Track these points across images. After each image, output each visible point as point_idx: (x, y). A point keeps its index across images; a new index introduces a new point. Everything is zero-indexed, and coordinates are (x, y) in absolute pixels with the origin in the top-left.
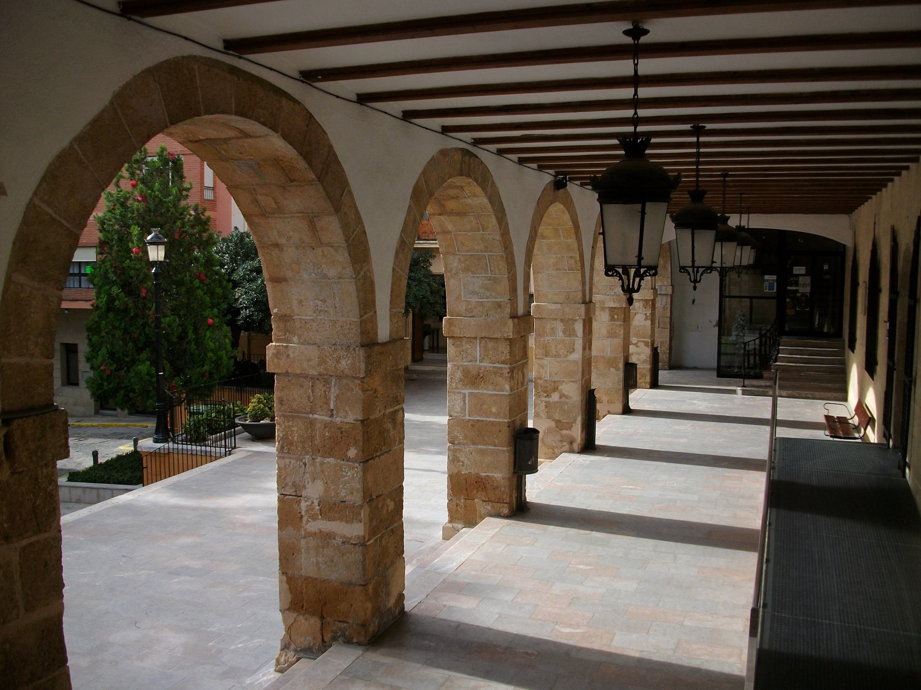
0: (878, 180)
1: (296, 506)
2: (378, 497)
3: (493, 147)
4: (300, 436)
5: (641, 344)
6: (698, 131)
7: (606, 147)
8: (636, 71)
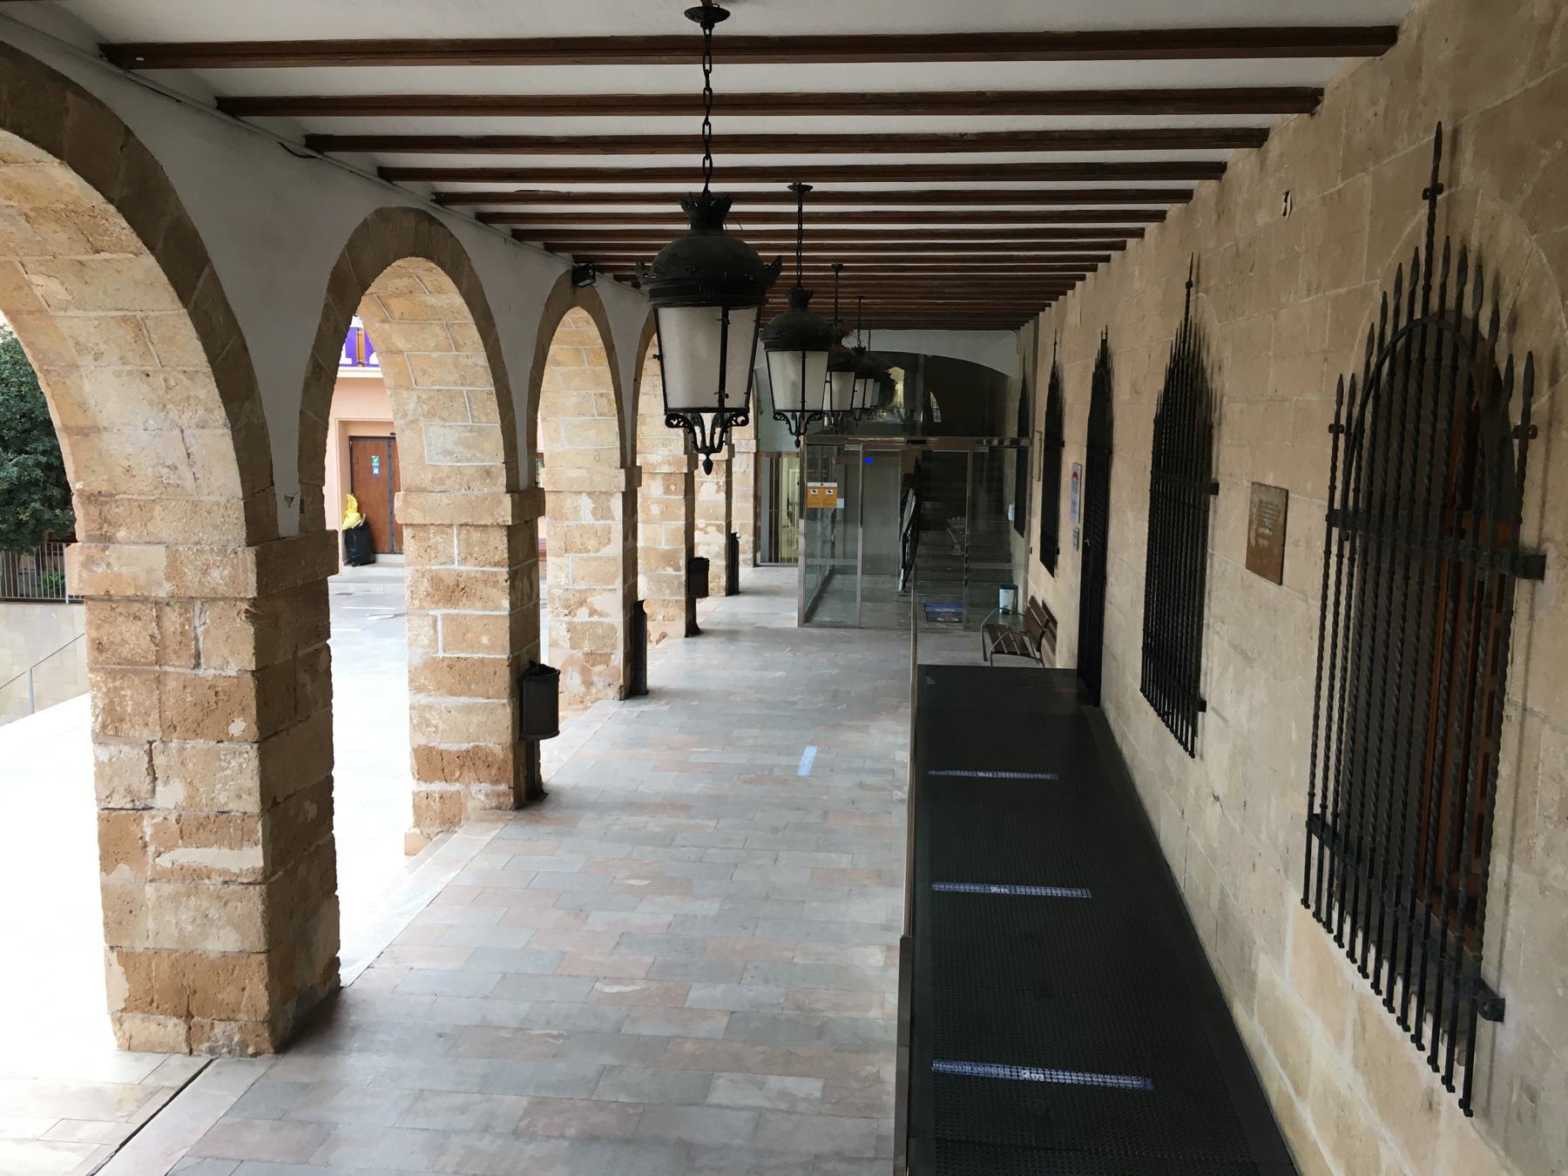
0: (1060, 277)
1: (134, 828)
2: (288, 798)
3: (467, 210)
4: (137, 704)
5: (711, 529)
6: (801, 195)
7: (659, 210)
8: (708, 88)
